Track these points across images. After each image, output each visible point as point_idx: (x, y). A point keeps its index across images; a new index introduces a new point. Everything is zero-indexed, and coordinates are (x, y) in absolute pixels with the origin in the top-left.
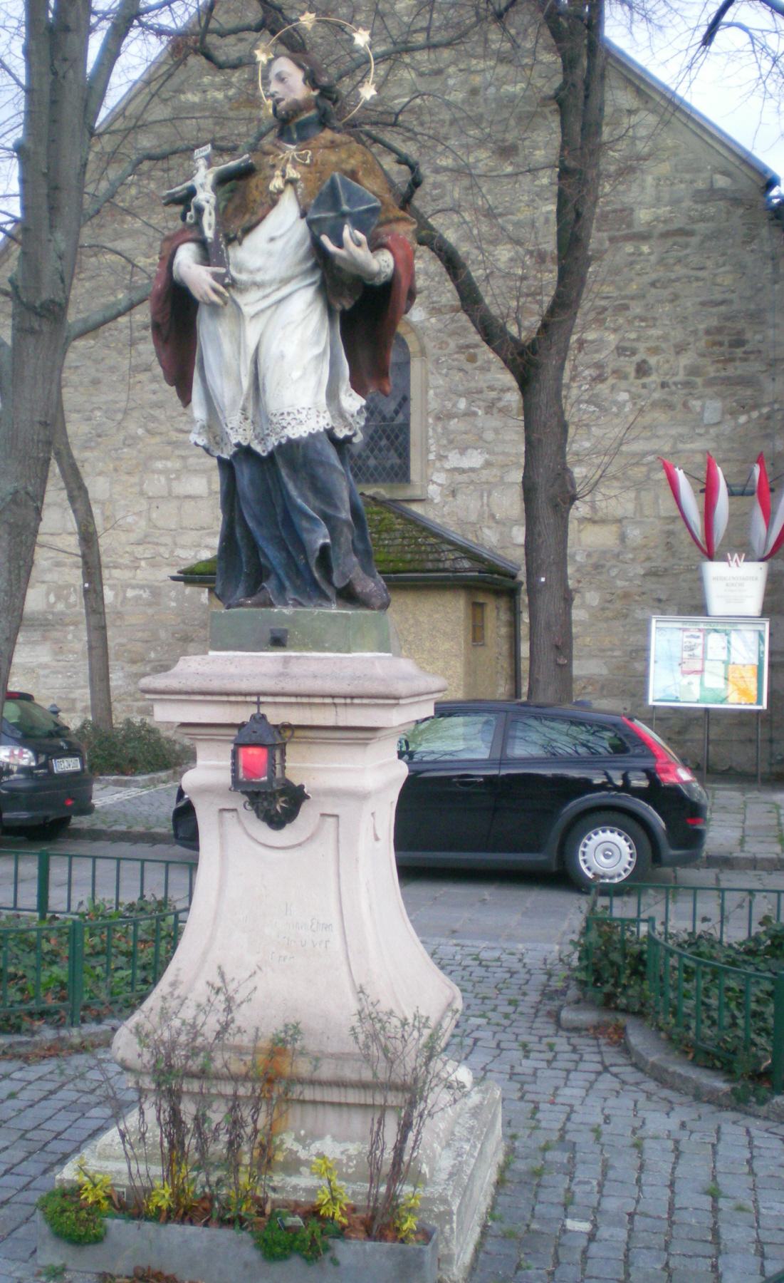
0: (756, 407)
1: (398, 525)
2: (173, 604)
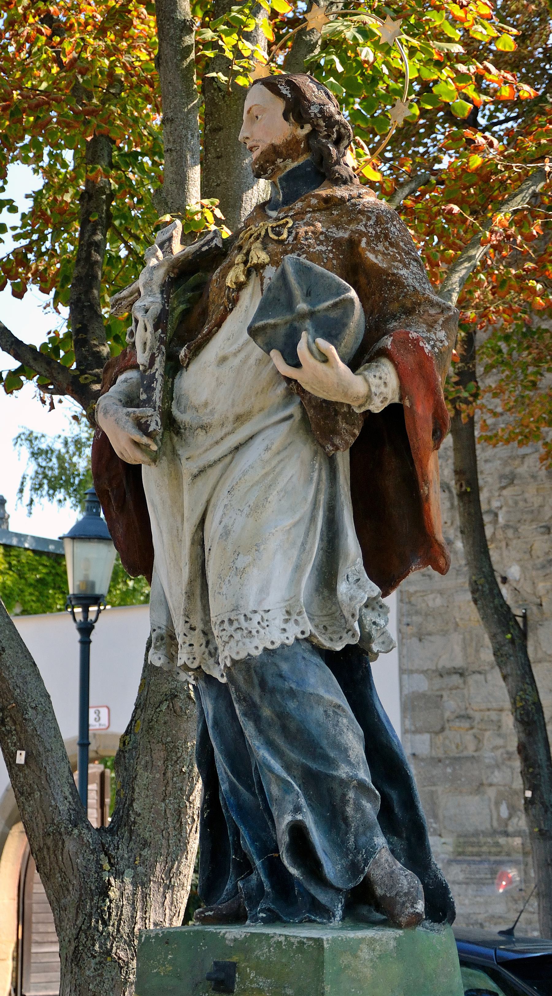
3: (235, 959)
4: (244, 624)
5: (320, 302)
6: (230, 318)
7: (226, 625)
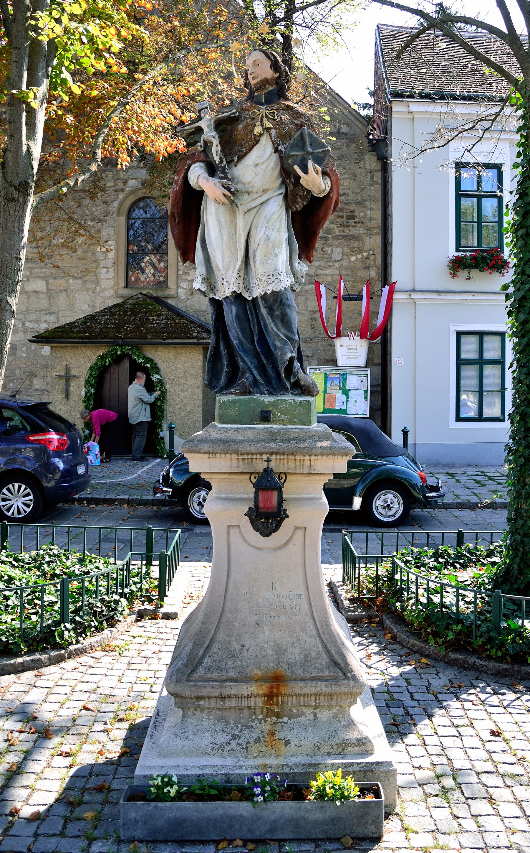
0: (361, 252)
1: (164, 312)
2: (24, 355)
3: (270, 409)
4: (279, 277)
5: (315, 149)
6: (255, 148)
7: (271, 277)
